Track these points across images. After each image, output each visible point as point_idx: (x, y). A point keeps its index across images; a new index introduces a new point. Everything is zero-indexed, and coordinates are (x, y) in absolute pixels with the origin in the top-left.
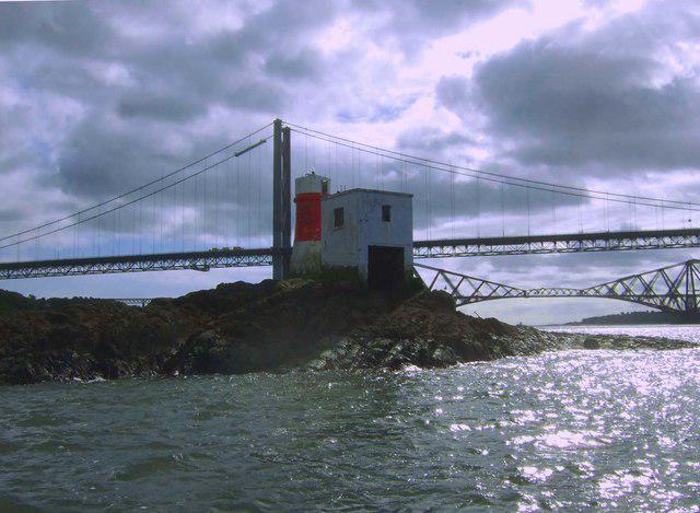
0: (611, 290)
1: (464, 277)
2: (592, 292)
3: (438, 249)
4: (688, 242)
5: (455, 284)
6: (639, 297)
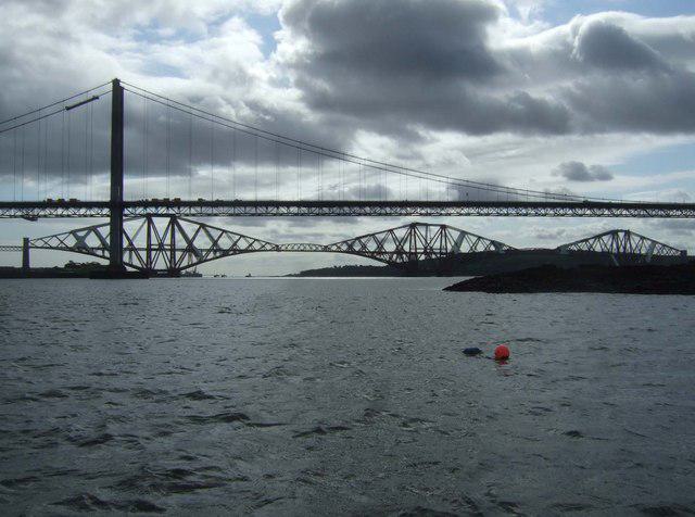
0: (350, 247)
1: (224, 231)
2: (334, 248)
3: (199, 209)
4: (383, 211)
5: (190, 236)
6: (373, 253)
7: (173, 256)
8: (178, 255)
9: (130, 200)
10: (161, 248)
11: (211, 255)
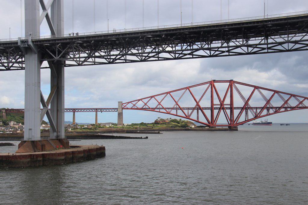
7: (232, 112)
8: (236, 112)
9: (160, 57)
10: (222, 107)
11: (265, 112)
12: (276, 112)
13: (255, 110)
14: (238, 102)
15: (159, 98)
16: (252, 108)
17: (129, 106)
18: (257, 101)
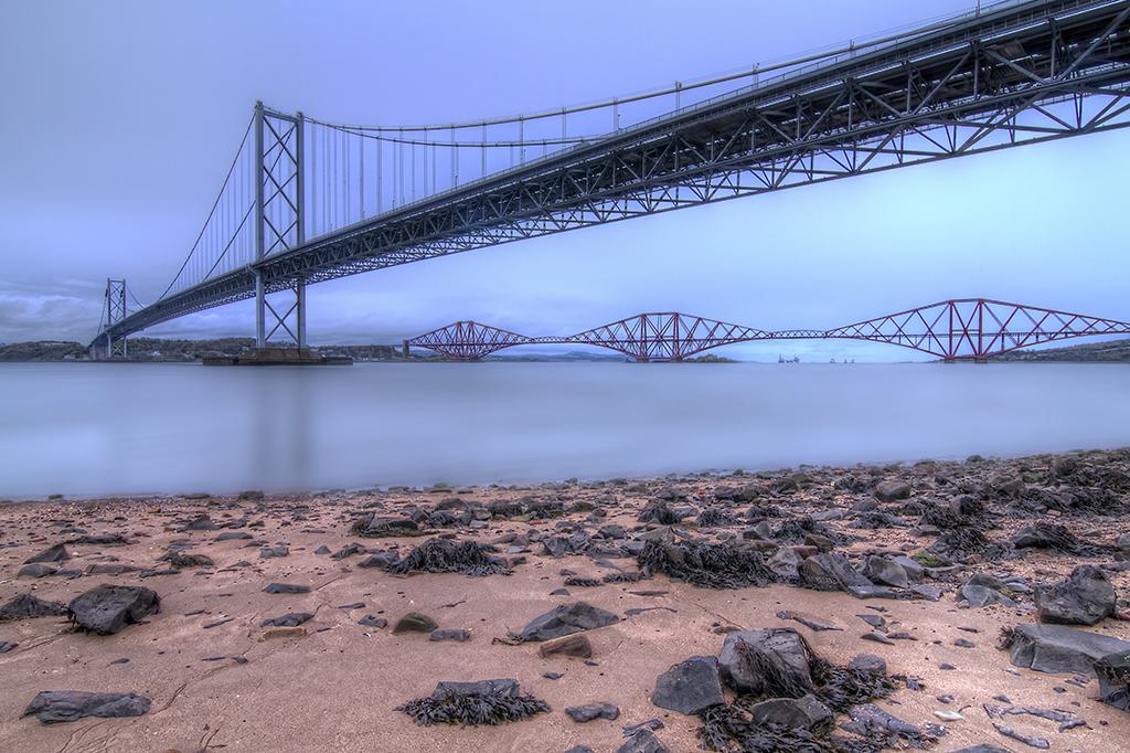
8: (986, 341)
11: (1032, 339)
12: (1051, 339)
13: (1016, 338)
14: (683, 335)
15: (900, 320)
16: (1010, 335)
17: (838, 333)
18: (701, 333)
